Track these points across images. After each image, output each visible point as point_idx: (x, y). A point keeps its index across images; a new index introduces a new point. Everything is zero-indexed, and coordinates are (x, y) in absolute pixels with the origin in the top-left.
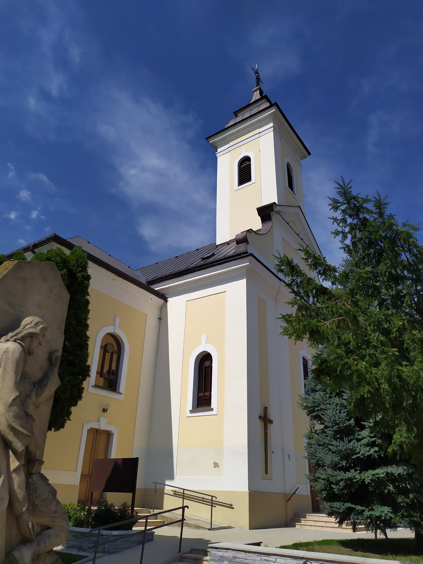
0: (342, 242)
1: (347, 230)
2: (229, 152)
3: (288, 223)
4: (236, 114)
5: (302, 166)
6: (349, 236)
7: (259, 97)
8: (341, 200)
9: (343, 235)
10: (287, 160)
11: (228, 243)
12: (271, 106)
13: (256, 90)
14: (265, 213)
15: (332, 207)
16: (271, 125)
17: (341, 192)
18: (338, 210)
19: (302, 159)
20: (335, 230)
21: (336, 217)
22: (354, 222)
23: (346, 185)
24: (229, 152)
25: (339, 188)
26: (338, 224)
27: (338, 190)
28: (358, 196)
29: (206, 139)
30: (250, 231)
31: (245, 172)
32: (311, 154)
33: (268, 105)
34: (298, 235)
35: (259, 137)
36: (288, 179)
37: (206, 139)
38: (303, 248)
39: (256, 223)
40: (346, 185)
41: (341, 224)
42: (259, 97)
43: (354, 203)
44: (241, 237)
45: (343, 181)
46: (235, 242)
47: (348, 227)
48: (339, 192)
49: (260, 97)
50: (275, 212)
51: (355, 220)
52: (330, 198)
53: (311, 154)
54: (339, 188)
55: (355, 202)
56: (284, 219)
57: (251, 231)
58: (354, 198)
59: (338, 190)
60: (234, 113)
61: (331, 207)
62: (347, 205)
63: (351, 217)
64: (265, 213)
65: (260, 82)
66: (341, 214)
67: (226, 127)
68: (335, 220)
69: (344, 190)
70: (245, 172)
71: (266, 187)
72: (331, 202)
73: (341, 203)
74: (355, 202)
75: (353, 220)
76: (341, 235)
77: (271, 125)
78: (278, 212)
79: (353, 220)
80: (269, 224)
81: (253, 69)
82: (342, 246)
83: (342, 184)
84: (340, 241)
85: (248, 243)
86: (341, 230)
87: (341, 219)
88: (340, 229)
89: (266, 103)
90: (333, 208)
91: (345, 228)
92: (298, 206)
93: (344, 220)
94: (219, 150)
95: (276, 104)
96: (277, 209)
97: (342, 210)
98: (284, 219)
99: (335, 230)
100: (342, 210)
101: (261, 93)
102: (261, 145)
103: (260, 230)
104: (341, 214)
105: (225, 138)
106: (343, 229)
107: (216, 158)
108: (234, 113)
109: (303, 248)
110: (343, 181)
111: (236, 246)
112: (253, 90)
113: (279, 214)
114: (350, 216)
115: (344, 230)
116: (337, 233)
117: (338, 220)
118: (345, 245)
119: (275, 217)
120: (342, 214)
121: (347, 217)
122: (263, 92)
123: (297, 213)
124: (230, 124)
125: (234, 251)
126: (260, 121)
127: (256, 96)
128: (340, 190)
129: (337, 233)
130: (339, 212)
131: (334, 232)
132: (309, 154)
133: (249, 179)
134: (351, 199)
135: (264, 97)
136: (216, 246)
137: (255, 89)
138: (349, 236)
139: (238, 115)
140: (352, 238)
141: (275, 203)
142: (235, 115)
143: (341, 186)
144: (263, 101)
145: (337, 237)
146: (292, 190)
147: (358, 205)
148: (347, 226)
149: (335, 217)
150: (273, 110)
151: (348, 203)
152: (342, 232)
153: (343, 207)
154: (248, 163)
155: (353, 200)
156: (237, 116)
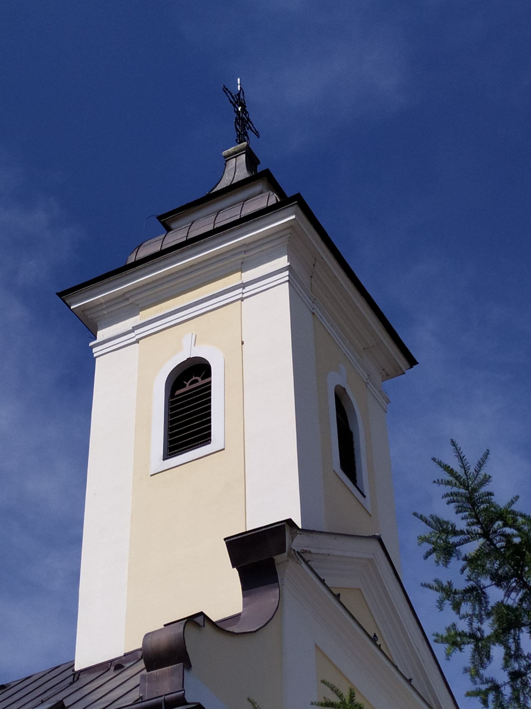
0: (475, 673)
1: (488, 628)
2: (137, 341)
3: (337, 597)
4: (166, 221)
5: (388, 402)
6: (497, 652)
7: (243, 173)
8: (461, 525)
9: (477, 649)
10: (334, 380)
11: (117, 665)
12: (284, 202)
13: (235, 154)
14: (256, 555)
15: (431, 547)
16: (283, 261)
17: (456, 494)
18: (453, 560)
19: (387, 376)
20: (448, 629)
21: (450, 584)
22: (510, 602)
23: (472, 470)
24: (137, 341)
25: (448, 483)
26: (456, 607)
27: (449, 489)
28: (514, 507)
29: (60, 295)
30: (197, 620)
31: (188, 410)
32: (416, 363)
33: (273, 199)
34: (374, 639)
35: (242, 299)
36: (337, 440)
37: (60, 295)
38: (340, 696)
39: (223, 594)
40: (472, 470)
41: (466, 608)
42: (243, 173)
43: (504, 535)
44: (164, 640)
45: (461, 459)
46: (142, 665)
47: (490, 621)
48: (452, 494)
49: (248, 175)
50: (289, 555)
51: (513, 595)
52: (421, 517)
53: (416, 363)
54: (448, 483)
55: (508, 530)
56: (323, 581)
57: (200, 620)
58: (501, 515)
59: (449, 489)
60: (160, 218)
61: (429, 547)
62: (482, 540)
63: (498, 585)
64: (256, 555)
65: (249, 132)
66: (462, 571)
67: (131, 259)
68: (447, 591)
69: (467, 487)
70: (188, 410)
71: (259, 464)
72: (426, 530)
73: (462, 532)
74: (508, 530)
75: (508, 595)
76: (469, 648)
77: (283, 261)
78: (301, 556)
79: (508, 595)
80: (268, 599)
81: (225, 90)
82: (472, 688)
83: (460, 471)
84: (466, 670)
85: (188, 665)
86: (467, 630)
87: (466, 591)
88: (463, 626)
89: (266, 194)
90: (434, 550)
91: (481, 621)
92: (374, 537)
93: (476, 594)
94: (102, 334)
95: (299, 201)
96: (297, 543)
97: (465, 559)
98: (323, 581)
99: (448, 629)
100: (465, 559)
101: (252, 161)
102: (247, 325)
103: (235, 618)
104: (462, 571)
105: (124, 297)
106: (476, 625)
107: (92, 361)
108: (160, 218)
109: (340, 696)
110: (461, 459)
111: (143, 677)
112: (225, 153)
113: (307, 563)
114: (499, 580)
115: (479, 629)
116: (455, 640)
117: (456, 593)
118: (487, 682)
119: (289, 571)
120: (467, 571)
121: (486, 581)
122: (258, 162)
123: (371, 560)
124: (143, 253)
125: (135, 695)
126: (246, 247)
127: (237, 170)
128: (455, 489)
129: (455, 640)
130: (456, 564)
131: (444, 634)
132: (412, 362)
133: (205, 437)
134: (492, 522)
135: (259, 175)
136: (77, 675)
137: (231, 150)
138: (497, 652)
139: (173, 226)
140: (509, 657)
141: (289, 522)
142: (163, 224)
143: (457, 478)
144: (258, 187)
145: (456, 654)
146: (354, 480)
147: (517, 540)
148: (489, 615)
149: (445, 584)
150: (288, 217)
151: (485, 534)
152: (472, 636)
153: (471, 548)
154: (201, 382)
155: (500, 523)
156: (169, 229)
